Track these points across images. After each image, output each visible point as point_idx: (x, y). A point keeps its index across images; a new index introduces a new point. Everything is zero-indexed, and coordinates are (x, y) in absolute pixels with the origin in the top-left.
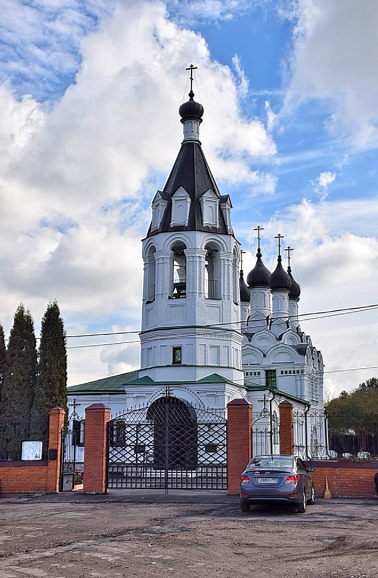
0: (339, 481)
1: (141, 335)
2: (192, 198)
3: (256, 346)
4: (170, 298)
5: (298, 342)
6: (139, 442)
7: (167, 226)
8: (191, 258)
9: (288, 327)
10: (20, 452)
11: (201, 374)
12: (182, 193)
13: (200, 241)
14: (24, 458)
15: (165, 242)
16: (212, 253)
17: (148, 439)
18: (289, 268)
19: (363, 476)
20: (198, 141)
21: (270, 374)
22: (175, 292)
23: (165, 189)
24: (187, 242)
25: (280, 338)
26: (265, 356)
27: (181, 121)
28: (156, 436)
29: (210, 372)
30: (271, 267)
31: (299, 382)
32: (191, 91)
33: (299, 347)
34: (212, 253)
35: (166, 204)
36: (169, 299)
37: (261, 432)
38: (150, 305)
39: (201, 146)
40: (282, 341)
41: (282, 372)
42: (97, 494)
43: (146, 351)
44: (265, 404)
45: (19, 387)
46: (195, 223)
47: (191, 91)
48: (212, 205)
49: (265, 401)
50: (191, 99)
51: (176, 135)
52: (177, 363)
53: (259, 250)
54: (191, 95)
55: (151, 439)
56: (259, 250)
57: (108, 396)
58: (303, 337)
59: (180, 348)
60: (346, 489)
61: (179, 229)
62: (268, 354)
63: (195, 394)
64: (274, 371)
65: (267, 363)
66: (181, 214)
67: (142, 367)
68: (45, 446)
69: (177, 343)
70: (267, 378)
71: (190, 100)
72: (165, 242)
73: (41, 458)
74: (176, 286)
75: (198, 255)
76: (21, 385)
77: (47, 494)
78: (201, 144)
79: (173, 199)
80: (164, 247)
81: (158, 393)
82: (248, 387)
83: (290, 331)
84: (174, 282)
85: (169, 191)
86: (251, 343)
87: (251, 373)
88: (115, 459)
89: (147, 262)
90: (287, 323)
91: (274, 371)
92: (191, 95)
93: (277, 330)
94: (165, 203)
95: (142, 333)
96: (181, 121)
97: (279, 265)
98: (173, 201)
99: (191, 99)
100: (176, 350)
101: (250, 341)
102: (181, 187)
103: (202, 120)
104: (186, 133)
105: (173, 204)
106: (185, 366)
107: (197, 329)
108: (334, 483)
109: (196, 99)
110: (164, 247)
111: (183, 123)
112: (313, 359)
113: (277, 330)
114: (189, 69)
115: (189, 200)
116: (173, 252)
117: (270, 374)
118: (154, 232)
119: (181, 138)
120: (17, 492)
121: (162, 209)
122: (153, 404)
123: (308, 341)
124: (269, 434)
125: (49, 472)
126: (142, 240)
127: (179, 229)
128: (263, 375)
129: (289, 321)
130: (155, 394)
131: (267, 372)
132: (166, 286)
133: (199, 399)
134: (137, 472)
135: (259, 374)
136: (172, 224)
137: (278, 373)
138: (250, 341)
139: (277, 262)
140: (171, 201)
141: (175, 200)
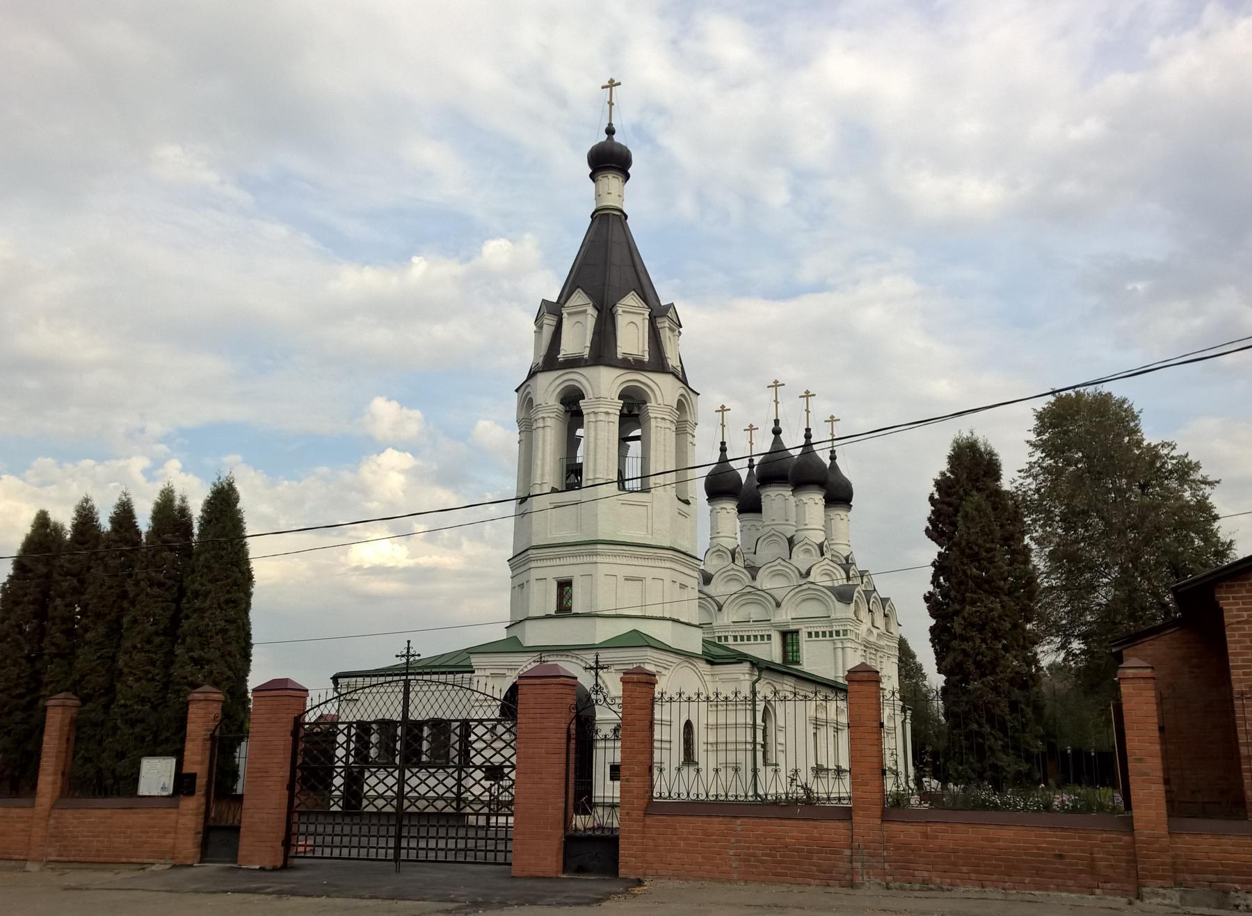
0: (742, 848)
2: (599, 308)
5: (840, 580)
7: (551, 361)
10: (135, 780)
11: (604, 631)
12: (579, 299)
13: (604, 386)
14: (140, 793)
15: (549, 388)
16: (633, 411)
19: (793, 837)
20: (621, 211)
21: (789, 637)
23: (560, 297)
25: (808, 573)
29: (624, 627)
30: (793, 441)
31: (839, 652)
32: (610, 124)
34: (633, 411)
40: (811, 579)
41: (810, 634)
42: (262, 869)
43: (519, 588)
45: (147, 647)
47: (610, 124)
48: (638, 319)
51: (580, 196)
52: (564, 609)
53: (777, 422)
54: (610, 131)
56: (777, 422)
58: (851, 573)
60: (756, 867)
61: (574, 363)
64: (797, 632)
65: (785, 616)
66: (576, 340)
68: (179, 765)
69: (564, 573)
70: (784, 644)
73: (171, 792)
76: (149, 642)
77: (174, 866)
78: (626, 217)
81: (526, 663)
85: (562, 301)
86: (757, 584)
87: (762, 636)
88: (423, 789)
92: (610, 131)
94: (550, 321)
97: (777, 440)
98: (565, 315)
100: (564, 586)
101: (754, 578)
105: (565, 321)
106: (577, 615)
107: (599, 546)
108: (732, 852)
112: (870, 611)
115: (592, 312)
116: (561, 407)
117: (789, 637)
120: (124, 860)
124: (749, 747)
125: (181, 821)
127: (574, 363)
128: (776, 639)
132: (547, 468)
135: (769, 637)
136: (561, 357)
137: (803, 636)
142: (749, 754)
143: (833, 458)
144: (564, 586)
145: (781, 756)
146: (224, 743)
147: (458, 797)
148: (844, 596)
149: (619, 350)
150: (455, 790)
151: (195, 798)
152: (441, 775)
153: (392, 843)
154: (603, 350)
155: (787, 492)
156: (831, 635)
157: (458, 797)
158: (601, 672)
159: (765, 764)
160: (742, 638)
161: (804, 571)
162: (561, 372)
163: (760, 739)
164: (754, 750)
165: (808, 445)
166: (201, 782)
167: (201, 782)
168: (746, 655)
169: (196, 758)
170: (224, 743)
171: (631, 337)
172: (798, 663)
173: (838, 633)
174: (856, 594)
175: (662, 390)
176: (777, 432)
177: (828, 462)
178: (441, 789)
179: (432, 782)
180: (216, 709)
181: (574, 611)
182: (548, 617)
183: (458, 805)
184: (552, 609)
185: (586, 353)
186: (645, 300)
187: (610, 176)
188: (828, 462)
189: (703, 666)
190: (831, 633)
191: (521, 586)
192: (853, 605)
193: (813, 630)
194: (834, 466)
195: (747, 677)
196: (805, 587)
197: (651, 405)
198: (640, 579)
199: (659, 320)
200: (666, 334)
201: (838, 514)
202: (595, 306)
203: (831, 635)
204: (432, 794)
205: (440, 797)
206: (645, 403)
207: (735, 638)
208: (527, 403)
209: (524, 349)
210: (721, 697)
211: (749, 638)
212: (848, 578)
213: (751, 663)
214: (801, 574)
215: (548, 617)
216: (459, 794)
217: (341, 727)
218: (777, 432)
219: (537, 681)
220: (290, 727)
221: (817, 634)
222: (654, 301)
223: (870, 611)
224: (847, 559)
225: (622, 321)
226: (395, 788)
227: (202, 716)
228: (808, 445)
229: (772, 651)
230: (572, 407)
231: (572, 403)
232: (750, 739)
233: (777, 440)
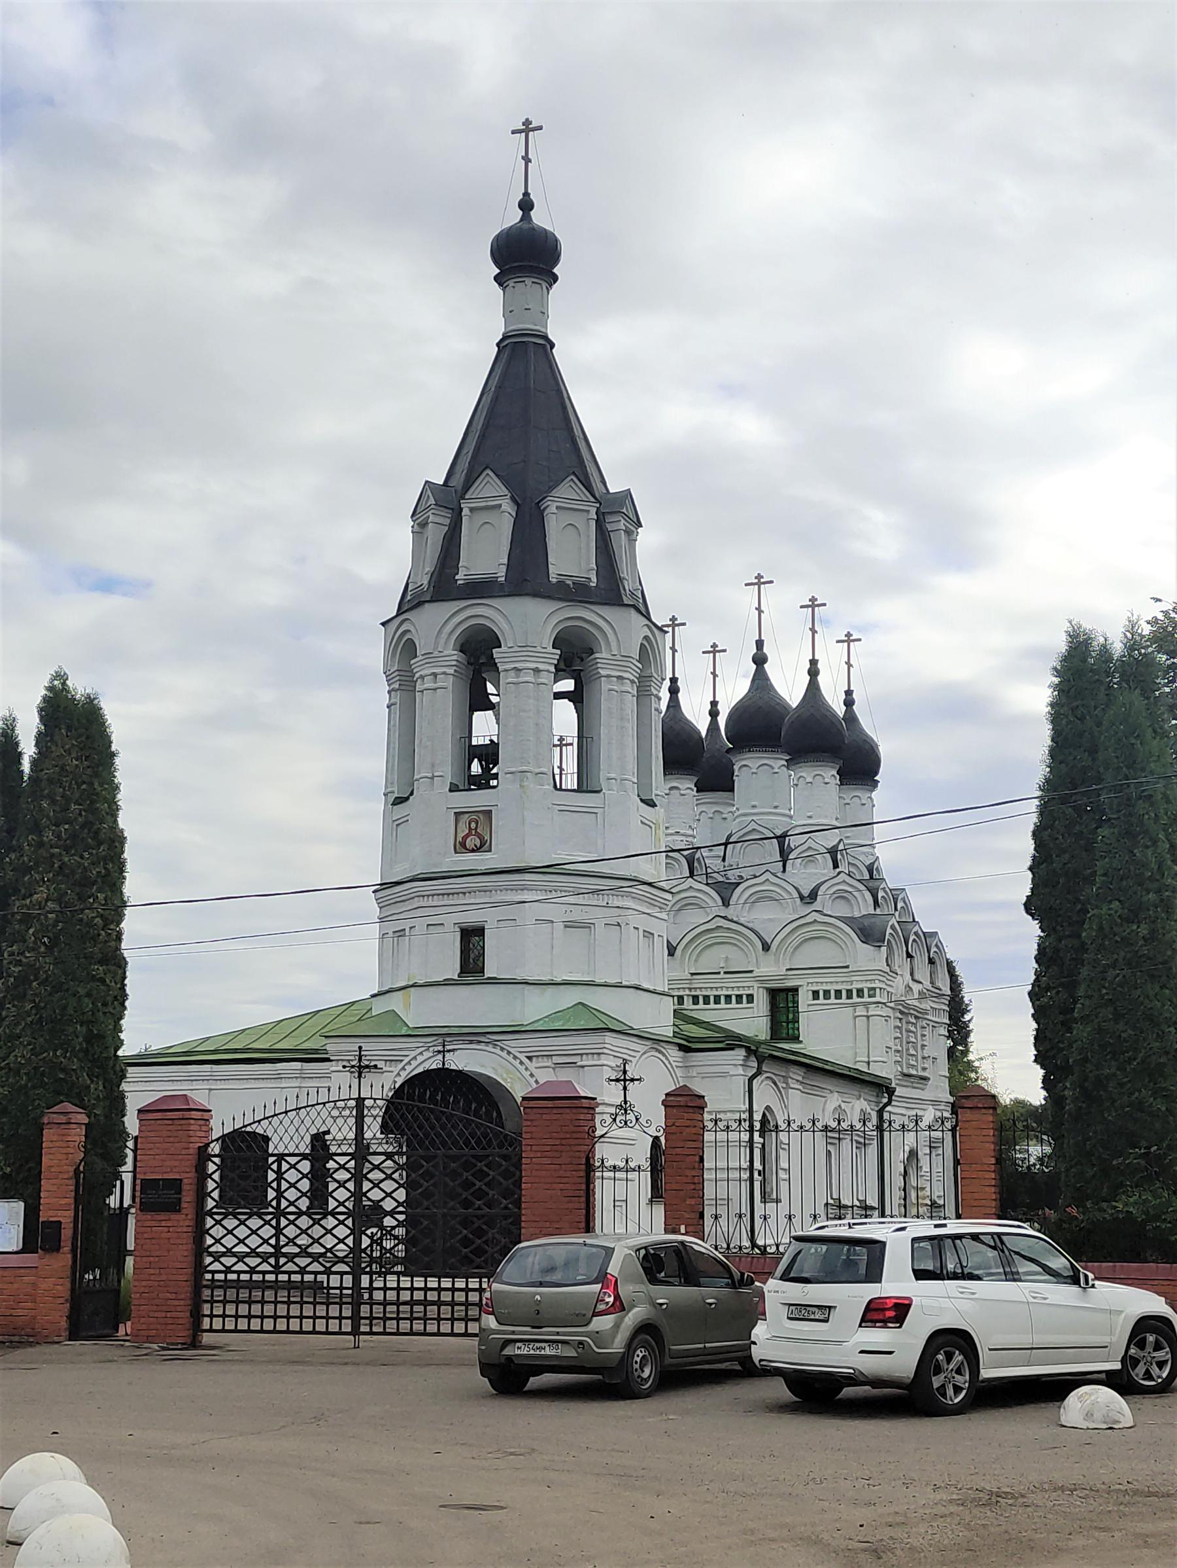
1: (379, 894)
3: (742, 920)
4: (454, 788)
5: (863, 906)
6: (284, 1204)
7: (440, 582)
8: (512, 673)
9: (836, 866)
12: (490, 488)
15: (440, 626)
17: (388, 1192)
18: (849, 693)
20: (546, 338)
21: (782, 1002)
22: (476, 768)
24: (502, 627)
25: (813, 895)
26: (766, 947)
27: (496, 278)
28: (409, 1186)
30: (790, 688)
31: (861, 1022)
32: (526, 194)
33: (866, 922)
34: (574, 657)
35: (448, 521)
36: (450, 791)
37: (615, 1168)
38: (402, 810)
39: (554, 351)
40: (817, 905)
41: (816, 994)
44: (625, 1088)
46: (526, 573)
47: (526, 194)
48: (577, 520)
49: (625, 1080)
50: (526, 217)
53: (760, 644)
54: (526, 205)
55: (401, 1195)
56: (760, 644)
57: (297, 1065)
58: (881, 894)
59: (480, 931)
61: (481, 589)
62: (776, 943)
63: (521, 1063)
64: (795, 990)
65: (771, 969)
66: (486, 551)
67: (381, 983)
69: (472, 918)
71: (521, 220)
72: (440, 626)
74: (475, 752)
75: (534, 665)
78: (552, 345)
79: (466, 506)
80: (436, 644)
82: (688, 1039)
83: (842, 877)
84: (474, 743)
85: (458, 481)
86: (730, 912)
87: (739, 997)
88: (229, 1241)
89: (396, 686)
90: (833, 852)
91: (795, 990)
92: (526, 205)
93: (803, 875)
94: (438, 523)
95: (384, 886)
96: (496, 278)
97: (760, 679)
98: (465, 512)
99: (526, 217)
100: (472, 936)
101: (726, 903)
102: (488, 471)
103: (555, 278)
104: (508, 313)
109: (539, 218)
110: (436, 644)
111: (500, 285)
112: (909, 956)
113: (803, 875)
114: (520, 131)
115: (508, 507)
116: (462, 657)
117: (782, 1002)
118: (414, 596)
119: (498, 329)
121: (436, 534)
122: (399, 1092)
123: (900, 905)
124: (745, 1175)
126: (383, 624)
127: (481, 589)
129: (841, 847)
130: (409, 1063)
131: (774, 994)
133: (532, 1075)
134: (398, 1289)
135: (750, 998)
136: (460, 577)
137: (804, 998)
138: (726, 903)
139: (709, 718)
140: (461, 509)
141: (472, 510)
142: (745, 1186)
143: (849, 703)
144: (472, 936)
145: (784, 1186)
146: (93, 1183)
147: (278, 1252)
148: (869, 934)
149: (553, 570)
150: (273, 1241)
151: (61, 1256)
152: (255, 1223)
153: (347, 1312)
154: (526, 573)
155: (778, 762)
156: (849, 996)
157: (278, 1252)
158: (630, 1086)
159: (764, 1200)
160: (706, 1000)
161: (806, 893)
162: (455, 606)
163: (757, 1165)
164: (751, 1179)
165: (813, 687)
166: (67, 1233)
167: (67, 1233)
168: (739, 1037)
169: (58, 1203)
170: (93, 1183)
171: (569, 554)
172: (796, 1039)
173: (860, 993)
174: (889, 931)
175: (617, 633)
176: (760, 660)
177: (840, 710)
178: (254, 1241)
179: (242, 1232)
180: (78, 1135)
181: (488, 973)
182: (447, 983)
183: (277, 1261)
184: (452, 970)
185: (501, 574)
186: (589, 488)
187: (528, 281)
188: (840, 710)
189: (674, 1054)
190: (849, 992)
191: (400, 933)
192: (884, 949)
193: (821, 988)
194: (850, 717)
195: (740, 1071)
196: (809, 919)
197: (602, 655)
198: (588, 926)
199: (609, 519)
200: (619, 541)
201: (855, 794)
202: (513, 499)
203: (849, 996)
204: (241, 1248)
205: (253, 1253)
206: (591, 652)
207: (695, 1000)
208: (403, 651)
209: (390, 557)
210: (819, 1125)
211: (717, 1000)
212: (876, 904)
213: (748, 1049)
214: (802, 898)
215: (447, 983)
216: (278, 1247)
217: (271, 1159)
218: (760, 660)
219: (550, 1104)
220: (193, 1160)
221: (827, 994)
222: (600, 485)
223: (909, 956)
224: (870, 869)
225: (555, 524)
226: (350, 1241)
227: (63, 1144)
228: (813, 687)
229: (753, 1022)
230: (479, 656)
231: (479, 656)
232: (745, 1165)
233: (760, 679)
